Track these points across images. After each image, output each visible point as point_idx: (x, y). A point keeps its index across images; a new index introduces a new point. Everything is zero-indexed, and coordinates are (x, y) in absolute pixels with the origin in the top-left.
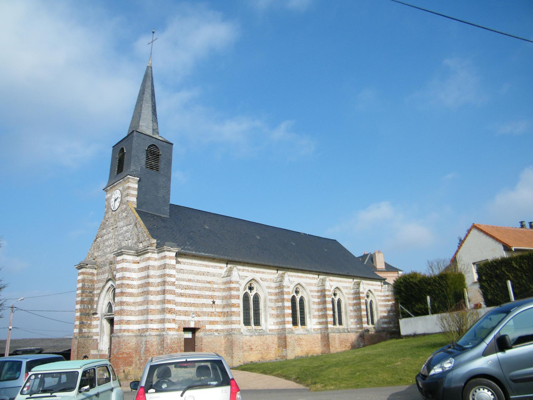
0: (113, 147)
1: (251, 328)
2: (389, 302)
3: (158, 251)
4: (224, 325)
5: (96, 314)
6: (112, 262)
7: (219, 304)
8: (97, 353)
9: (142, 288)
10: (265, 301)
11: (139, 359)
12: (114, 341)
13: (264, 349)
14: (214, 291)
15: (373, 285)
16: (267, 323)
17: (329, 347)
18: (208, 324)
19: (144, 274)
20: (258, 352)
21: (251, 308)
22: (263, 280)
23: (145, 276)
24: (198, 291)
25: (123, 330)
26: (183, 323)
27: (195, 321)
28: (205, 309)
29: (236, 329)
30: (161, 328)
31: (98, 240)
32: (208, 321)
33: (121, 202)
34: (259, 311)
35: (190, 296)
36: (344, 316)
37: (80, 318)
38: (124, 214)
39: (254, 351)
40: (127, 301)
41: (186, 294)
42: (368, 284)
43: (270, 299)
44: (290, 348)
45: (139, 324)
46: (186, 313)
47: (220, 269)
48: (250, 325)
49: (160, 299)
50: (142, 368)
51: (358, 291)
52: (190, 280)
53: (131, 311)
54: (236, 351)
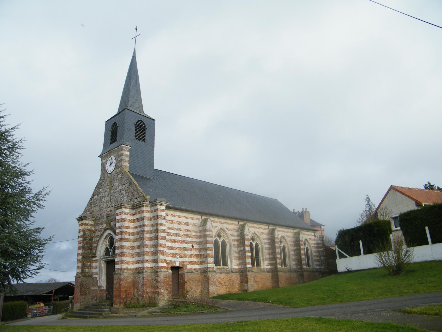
0: (105, 122)
1: (220, 267)
2: (320, 248)
3: (151, 205)
4: (201, 265)
5: (95, 257)
6: (109, 214)
7: (197, 248)
8: (97, 289)
9: (138, 235)
10: (230, 246)
11: (137, 292)
12: (116, 278)
13: (231, 284)
14: (192, 237)
15: (308, 235)
16: (232, 263)
17: (279, 283)
18: (189, 264)
19: (138, 224)
20: (226, 286)
21: (220, 252)
22: (228, 230)
23: (140, 225)
24: (181, 238)
25: (123, 269)
26: (170, 263)
27: (179, 261)
28: (186, 252)
29: (211, 267)
30: (155, 267)
31: (95, 197)
32: (189, 261)
33: (115, 166)
34: (226, 254)
35: (175, 241)
36: (287, 259)
37: (82, 260)
38: (119, 176)
39: (223, 285)
40: (126, 245)
41: (172, 239)
42: (305, 234)
43: (233, 245)
44: (250, 283)
45: (136, 264)
46: (173, 255)
47: (197, 220)
48: (219, 265)
49: (154, 244)
50: (140, 298)
51: (298, 239)
52: (175, 229)
53: (129, 253)
54: (211, 285)
